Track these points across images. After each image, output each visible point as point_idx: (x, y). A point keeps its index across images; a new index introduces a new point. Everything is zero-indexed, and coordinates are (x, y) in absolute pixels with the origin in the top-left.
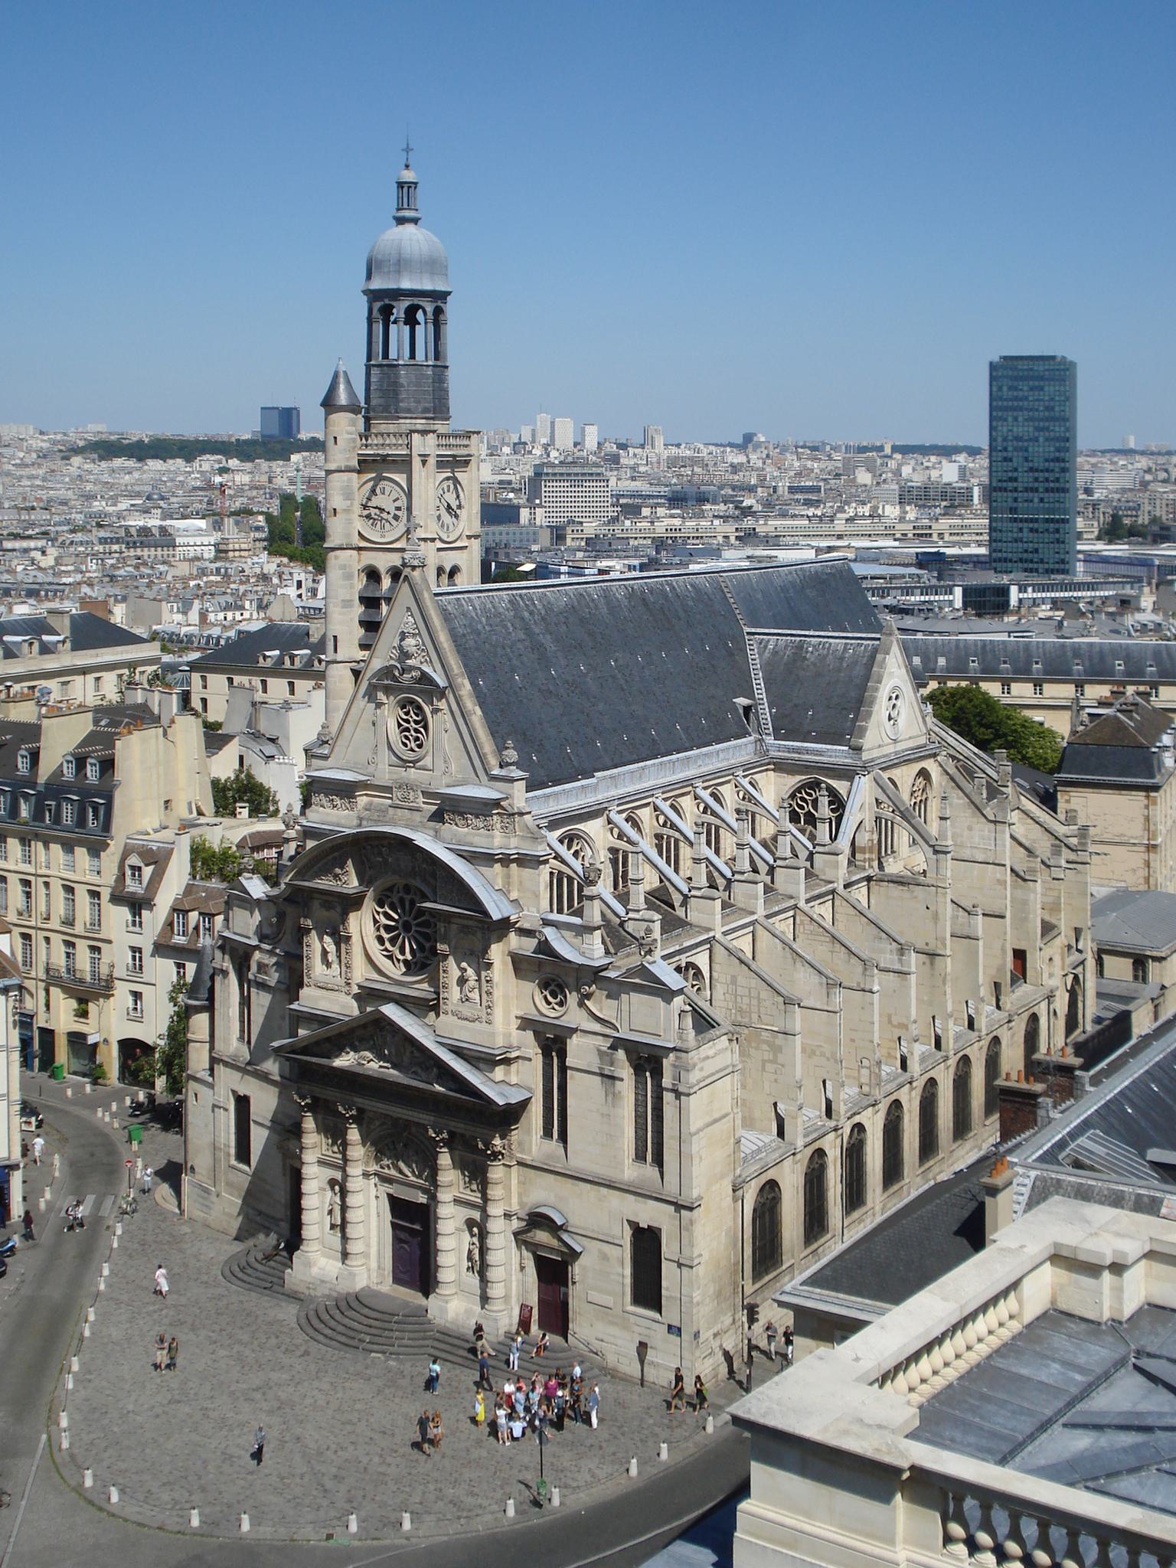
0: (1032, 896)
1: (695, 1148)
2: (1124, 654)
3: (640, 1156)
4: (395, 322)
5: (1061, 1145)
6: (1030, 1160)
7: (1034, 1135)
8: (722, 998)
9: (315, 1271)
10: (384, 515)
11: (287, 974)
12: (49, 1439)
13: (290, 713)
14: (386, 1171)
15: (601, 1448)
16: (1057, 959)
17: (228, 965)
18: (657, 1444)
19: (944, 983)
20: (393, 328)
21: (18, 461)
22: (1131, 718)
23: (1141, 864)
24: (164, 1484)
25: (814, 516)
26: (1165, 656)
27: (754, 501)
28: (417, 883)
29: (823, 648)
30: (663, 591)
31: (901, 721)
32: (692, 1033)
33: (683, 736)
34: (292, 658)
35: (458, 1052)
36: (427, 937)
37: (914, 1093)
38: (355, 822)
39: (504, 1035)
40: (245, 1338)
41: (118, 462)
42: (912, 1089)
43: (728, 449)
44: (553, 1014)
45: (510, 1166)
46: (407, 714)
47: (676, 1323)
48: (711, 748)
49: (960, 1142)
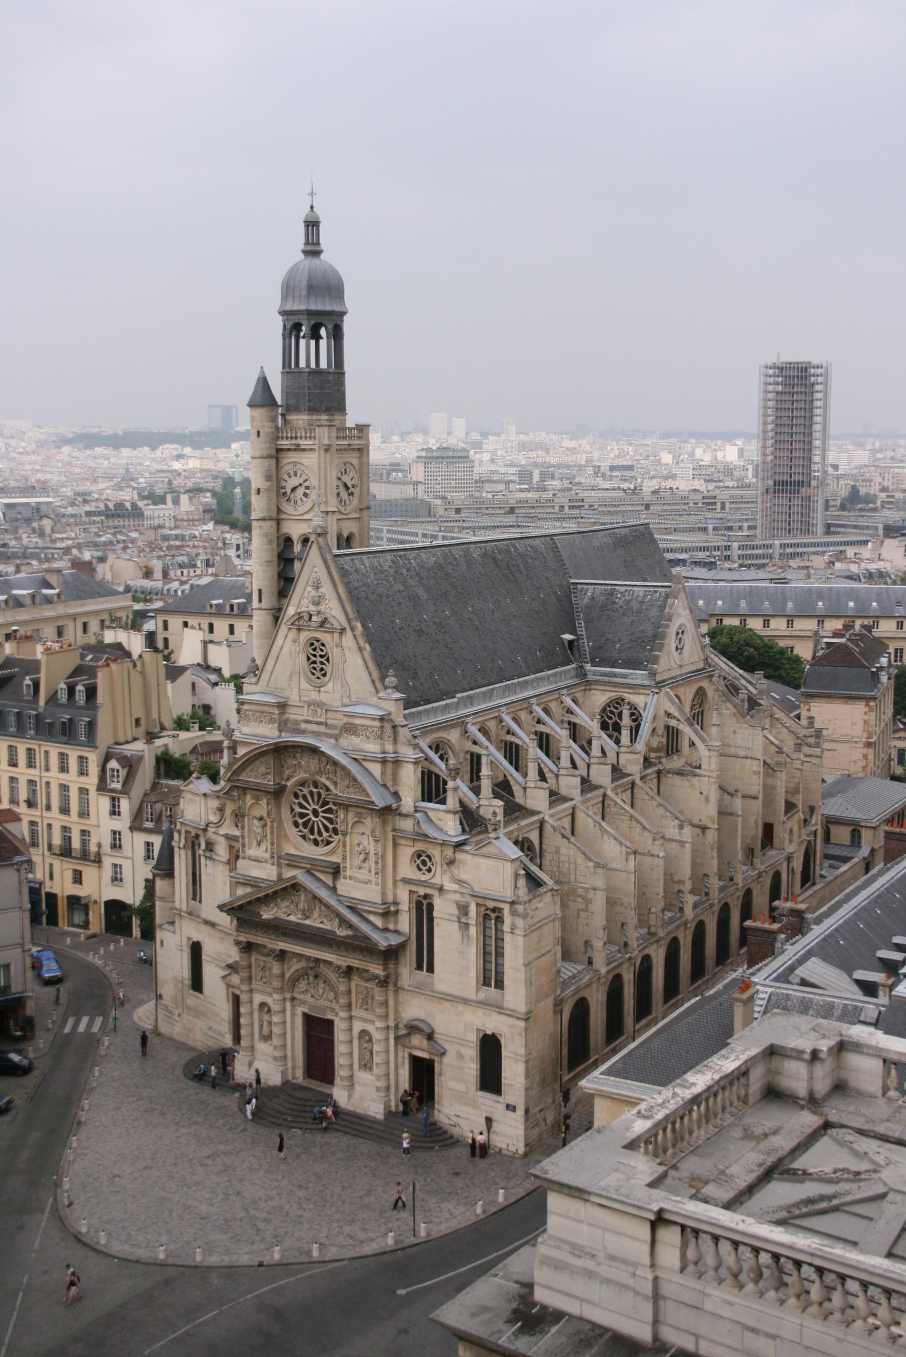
4: (304, 337)
5: (791, 969)
7: (771, 961)
12: (55, 1199)
15: (457, 1194)
16: (795, 829)
18: (497, 1190)
20: (302, 342)
21: (21, 450)
22: (858, 646)
23: (860, 757)
24: (140, 1229)
25: (629, 489)
26: (885, 595)
28: (323, 780)
31: (686, 651)
33: (523, 665)
36: (330, 821)
37: (688, 932)
40: (200, 1120)
41: (98, 450)
42: (685, 930)
43: (565, 436)
46: (314, 650)
49: (721, 967)
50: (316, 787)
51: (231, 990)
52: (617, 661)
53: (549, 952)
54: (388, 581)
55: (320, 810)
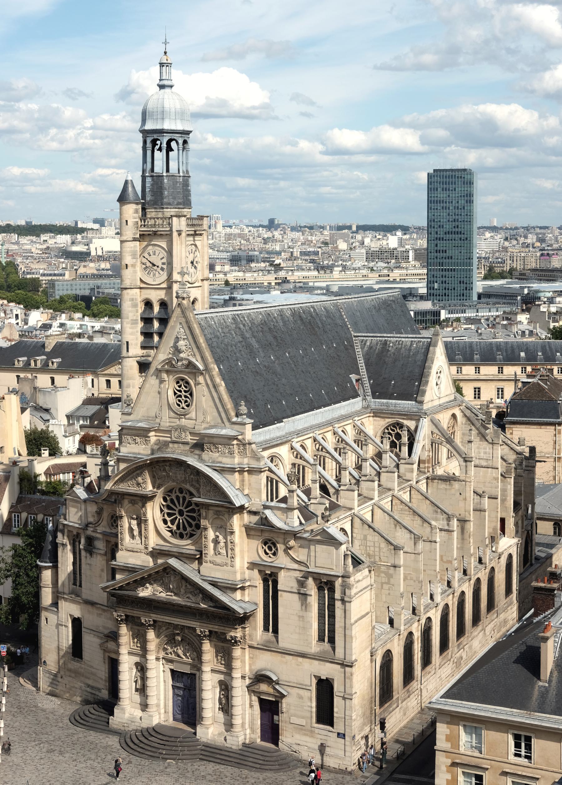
0: (509, 486)
1: (354, 632)
2: (525, 348)
3: (321, 639)
6: (558, 624)
8: (358, 548)
9: (127, 715)
10: (155, 268)
11: (105, 544)
13: (58, 393)
14: (170, 656)
17: (66, 541)
19: (470, 537)
22: (546, 384)
26: (547, 347)
27: (281, 261)
28: (188, 487)
29: (399, 344)
30: (310, 311)
31: (442, 386)
32: (351, 567)
34: (35, 361)
35: (214, 584)
36: (193, 518)
38: (149, 452)
39: (241, 573)
44: (269, 560)
45: (245, 649)
46: (180, 386)
47: (342, 732)
48: (339, 404)
49: (475, 627)
50: (181, 493)
51: (107, 654)
52: (393, 394)
53: (367, 614)
54: (231, 334)
55: (185, 510)
